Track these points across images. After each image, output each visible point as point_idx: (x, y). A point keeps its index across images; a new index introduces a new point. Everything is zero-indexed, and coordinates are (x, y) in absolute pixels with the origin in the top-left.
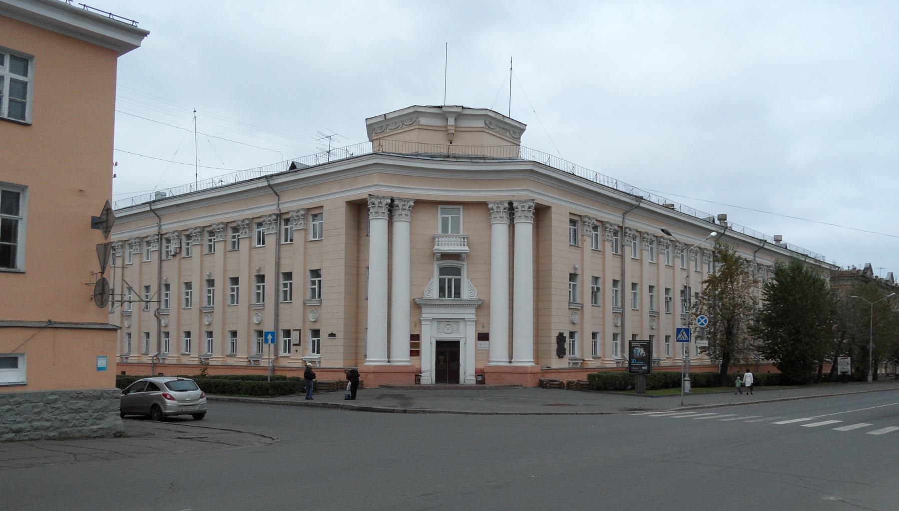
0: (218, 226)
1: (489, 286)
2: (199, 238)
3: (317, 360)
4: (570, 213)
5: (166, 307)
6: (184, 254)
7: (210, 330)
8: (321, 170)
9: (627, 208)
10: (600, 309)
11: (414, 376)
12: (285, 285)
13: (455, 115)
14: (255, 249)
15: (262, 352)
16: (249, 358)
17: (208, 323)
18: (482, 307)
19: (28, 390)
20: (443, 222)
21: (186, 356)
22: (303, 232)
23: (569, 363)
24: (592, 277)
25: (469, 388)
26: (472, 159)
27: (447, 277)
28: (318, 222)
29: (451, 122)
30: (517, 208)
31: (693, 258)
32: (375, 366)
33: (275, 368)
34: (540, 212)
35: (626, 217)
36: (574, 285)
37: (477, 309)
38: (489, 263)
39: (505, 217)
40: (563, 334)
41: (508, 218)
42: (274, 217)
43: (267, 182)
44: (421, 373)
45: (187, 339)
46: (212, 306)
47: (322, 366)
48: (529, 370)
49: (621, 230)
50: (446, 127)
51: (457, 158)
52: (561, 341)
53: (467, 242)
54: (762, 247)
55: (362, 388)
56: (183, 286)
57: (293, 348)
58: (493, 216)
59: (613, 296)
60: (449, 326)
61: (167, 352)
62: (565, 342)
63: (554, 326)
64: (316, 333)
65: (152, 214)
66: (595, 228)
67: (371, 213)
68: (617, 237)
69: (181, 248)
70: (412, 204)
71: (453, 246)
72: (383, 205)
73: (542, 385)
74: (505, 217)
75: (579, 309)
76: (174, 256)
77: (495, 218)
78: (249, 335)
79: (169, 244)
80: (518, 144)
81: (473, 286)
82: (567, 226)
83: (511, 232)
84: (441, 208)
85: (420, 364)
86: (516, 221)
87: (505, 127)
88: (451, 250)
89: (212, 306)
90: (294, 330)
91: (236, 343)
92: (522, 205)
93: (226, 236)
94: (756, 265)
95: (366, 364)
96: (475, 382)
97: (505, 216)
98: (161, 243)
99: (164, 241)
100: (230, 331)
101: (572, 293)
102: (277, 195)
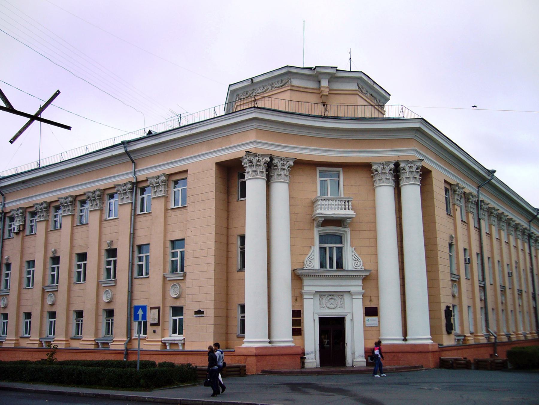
2: (45, 214)
3: (180, 342)
4: (446, 182)
5: (6, 287)
6: (27, 231)
7: (53, 310)
8: (187, 130)
11: (300, 358)
13: (329, 77)
14: (107, 222)
15: (81, 334)
16: (97, 340)
17: (51, 303)
21: (26, 340)
22: (163, 200)
25: (356, 372)
27: (328, 246)
28: (181, 188)
29: (324, 83)
30: (404, 169)
31: (520, 237)
32: (257, 348)
33: (129, 352)
39: (390, 179)
42: (130, 186)
44: (305, 356)
45: (27, 320)
46: (55, 284)
47: (187, 348)
48: (430, 349)
55: (245, 374)
56: (25, 265)
57: (150, 329)
58: (377, 178)
60: (333, 300)
61: (5, 335)
64: (178, 311)
67: (248, 172)
69: (24, 226)
70: (292, 163)
73: (444, 364)
74: (390, 179)
76: (17, 233)
77: (380, 180)
78: (97, 315)
79: (12, 223)
81: (358, 256)
84: (319, 171)
85: (303, 345)
87: (374, 94)
88: (336, 214)
89: (55, 284)
90: (152, 308)
92: (410, 165)
93: (74, 210)
95: (243, 345)
96: (364, 364)
99: (7, 220)
100: (76, 311)
102: (133, 162)
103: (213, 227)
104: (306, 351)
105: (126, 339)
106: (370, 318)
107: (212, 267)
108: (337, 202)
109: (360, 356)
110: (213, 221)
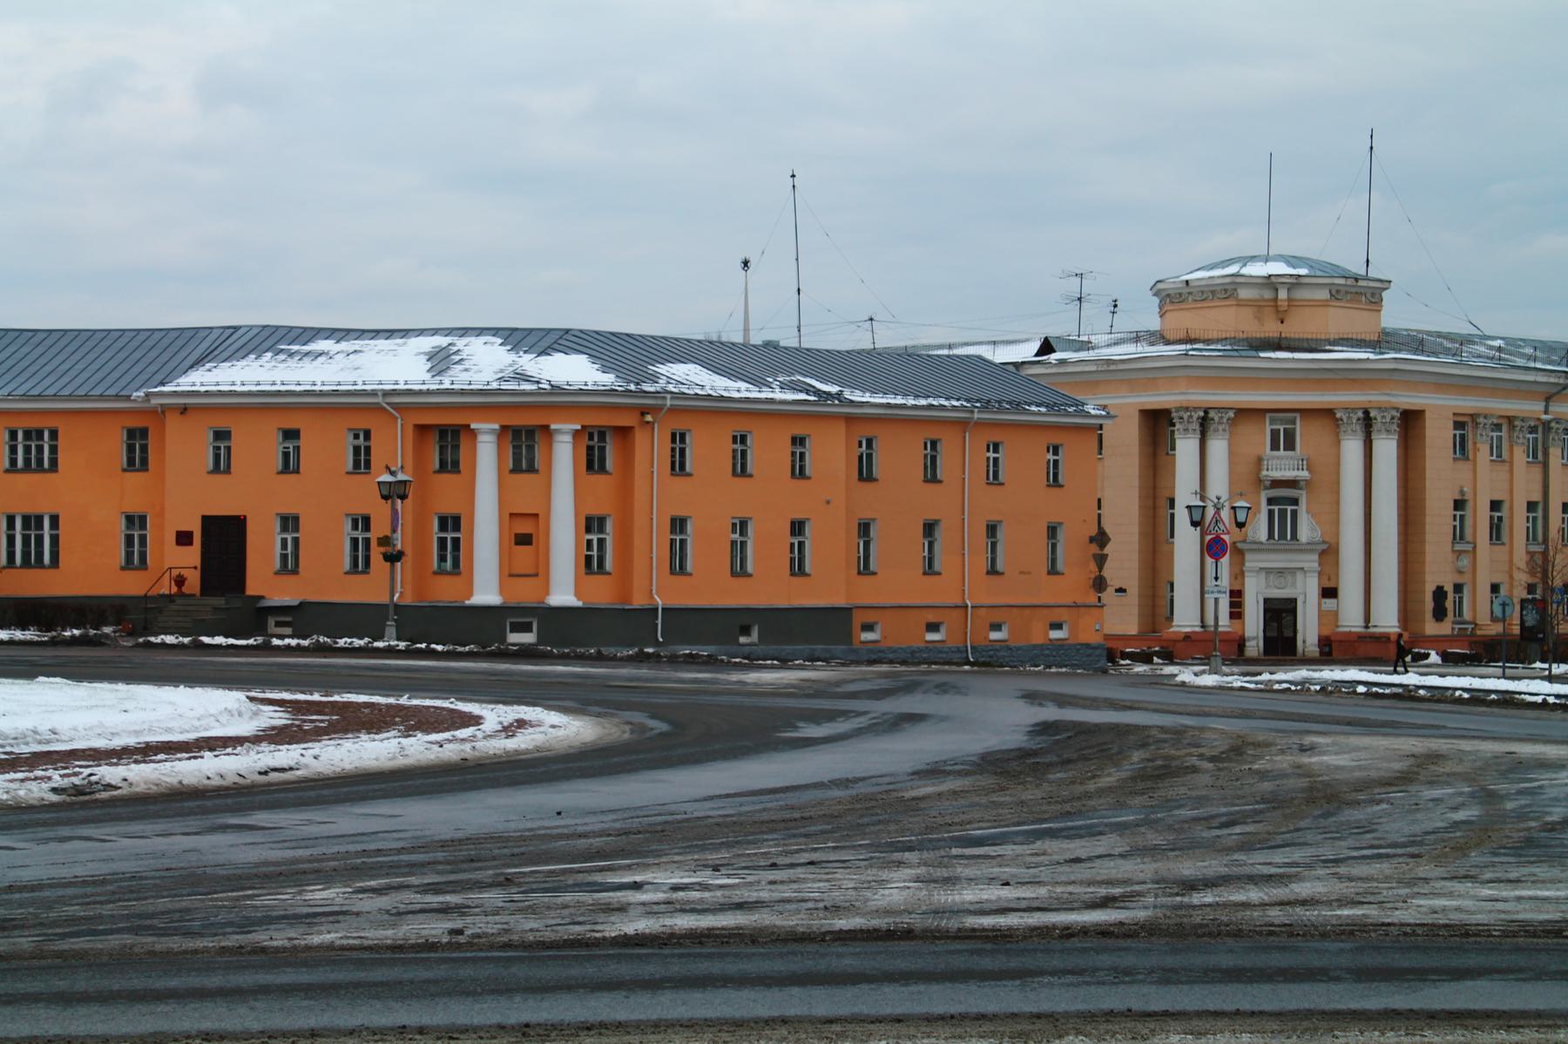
1: (1336, 522)
10: (1506, 549)
18: (1329, 553)
19: (1069, 642)
20: (1272, 435)
23: (1453, 629)
29: (1283, 294)
34: (1410, 422)
38: (1336, 491)
53: (1308, 465)
58: (1342, 429)
63: (1428, 577)
70: (1231, 414)
72: (1195, 419)
95: (1171, 630)
97: (1359, 428)
103: (1137, 490)
104: (1247, 635)
106: (1328, 601)
107: (1136, 538)
109: (1312, 645)
110: (1136, 482)
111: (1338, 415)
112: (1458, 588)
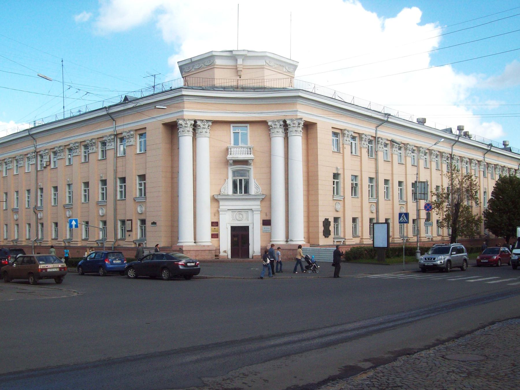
0: (74, 144)
4: (332, 128)
6: (52, 166)
9: (379, 123)
12: (121, 187)
23: (334, 241)
24: (369, 177)
26: (255, 89)
28: (143, 140)
35: (378, 130)
36: (337, 183)
37: (261, 201)
40: (328, 219)
41: (283, 132)
43: (106, 111)
46: (71, 203)
49: (374, 140)
50: (236, 66)
51: (244, 89)
52: (326, 225)
54: (490, 151)
58: (272, 131)
59: (399, 193)
62: (330, 225)
63: (320, 214)
64: (143, 222)
65: (30, 138)
66: (354, 138)
68: (372, 144)
69: (50, 161)
71: (242, 154)
74: (281, 132)
75: (341, 200)
80: (293, 76)
81: (258, 185)
82: (331, 137)
83: (286, 142)
84: (233, 126)
86: (289, 135)
90: (128, 220)
91: (88, 230)
94: (486, 164)
97: (281, 131)
98: (37, 159)
101: (400, 193)
105: (114, 240)
108: (245, 149)
111: (269, 124)
112: (336, 219)
